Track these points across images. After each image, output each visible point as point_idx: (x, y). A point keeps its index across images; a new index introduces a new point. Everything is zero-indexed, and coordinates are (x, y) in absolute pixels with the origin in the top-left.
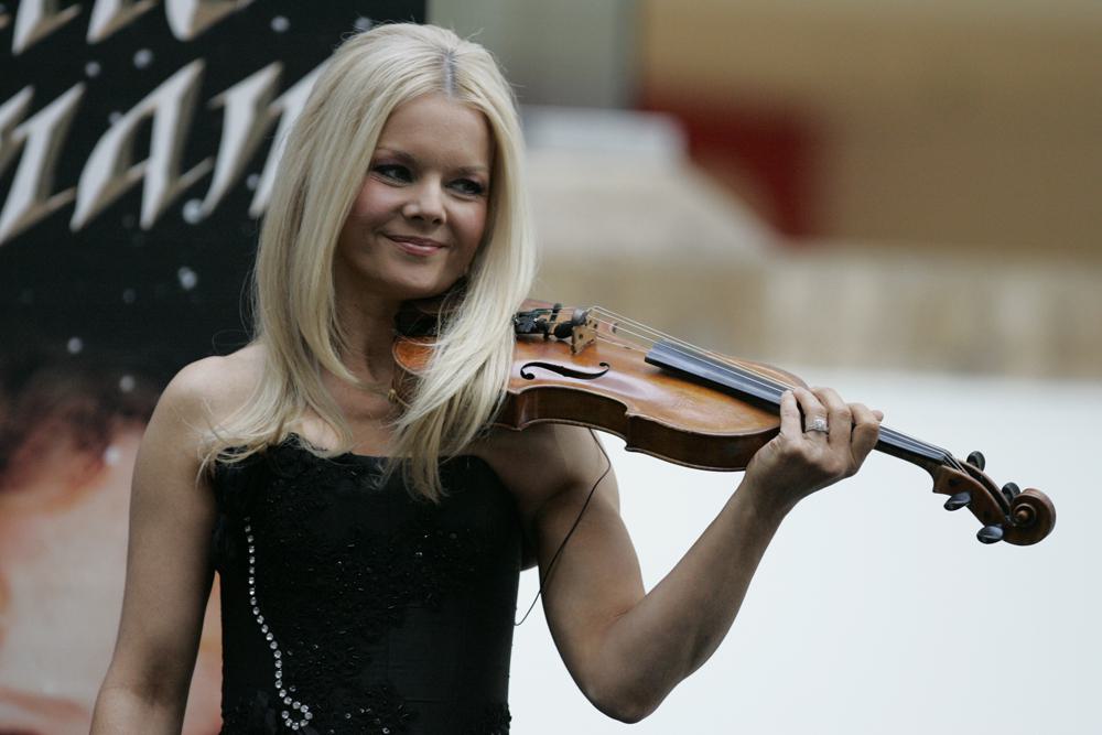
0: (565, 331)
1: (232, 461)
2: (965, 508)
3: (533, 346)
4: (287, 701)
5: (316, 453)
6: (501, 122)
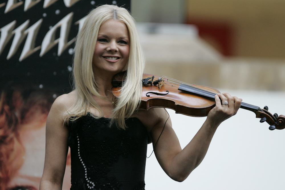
0: (156, 83)
1: (74, 120)
2: (265, 121)
3: (148, 88)
4: (88, 181)
5: (95, 117)
6: (130, 26)
